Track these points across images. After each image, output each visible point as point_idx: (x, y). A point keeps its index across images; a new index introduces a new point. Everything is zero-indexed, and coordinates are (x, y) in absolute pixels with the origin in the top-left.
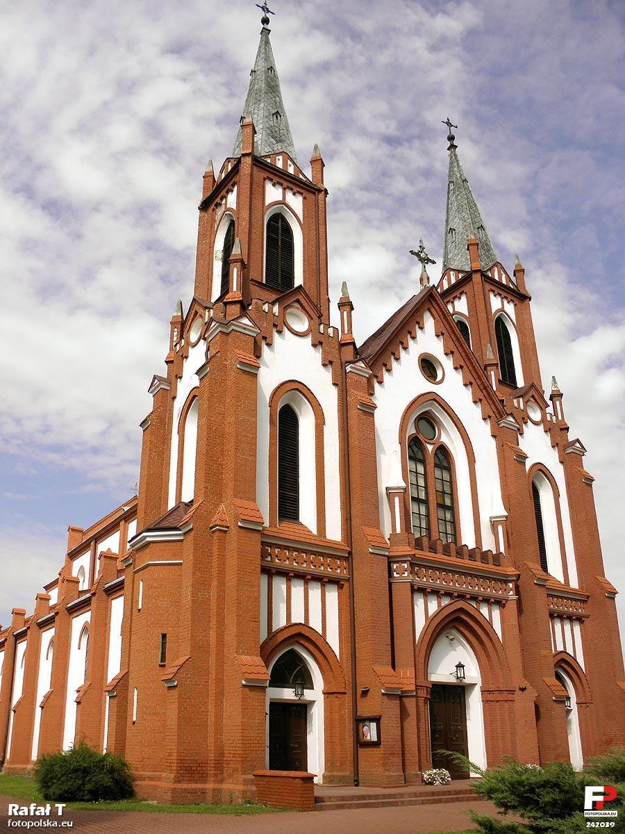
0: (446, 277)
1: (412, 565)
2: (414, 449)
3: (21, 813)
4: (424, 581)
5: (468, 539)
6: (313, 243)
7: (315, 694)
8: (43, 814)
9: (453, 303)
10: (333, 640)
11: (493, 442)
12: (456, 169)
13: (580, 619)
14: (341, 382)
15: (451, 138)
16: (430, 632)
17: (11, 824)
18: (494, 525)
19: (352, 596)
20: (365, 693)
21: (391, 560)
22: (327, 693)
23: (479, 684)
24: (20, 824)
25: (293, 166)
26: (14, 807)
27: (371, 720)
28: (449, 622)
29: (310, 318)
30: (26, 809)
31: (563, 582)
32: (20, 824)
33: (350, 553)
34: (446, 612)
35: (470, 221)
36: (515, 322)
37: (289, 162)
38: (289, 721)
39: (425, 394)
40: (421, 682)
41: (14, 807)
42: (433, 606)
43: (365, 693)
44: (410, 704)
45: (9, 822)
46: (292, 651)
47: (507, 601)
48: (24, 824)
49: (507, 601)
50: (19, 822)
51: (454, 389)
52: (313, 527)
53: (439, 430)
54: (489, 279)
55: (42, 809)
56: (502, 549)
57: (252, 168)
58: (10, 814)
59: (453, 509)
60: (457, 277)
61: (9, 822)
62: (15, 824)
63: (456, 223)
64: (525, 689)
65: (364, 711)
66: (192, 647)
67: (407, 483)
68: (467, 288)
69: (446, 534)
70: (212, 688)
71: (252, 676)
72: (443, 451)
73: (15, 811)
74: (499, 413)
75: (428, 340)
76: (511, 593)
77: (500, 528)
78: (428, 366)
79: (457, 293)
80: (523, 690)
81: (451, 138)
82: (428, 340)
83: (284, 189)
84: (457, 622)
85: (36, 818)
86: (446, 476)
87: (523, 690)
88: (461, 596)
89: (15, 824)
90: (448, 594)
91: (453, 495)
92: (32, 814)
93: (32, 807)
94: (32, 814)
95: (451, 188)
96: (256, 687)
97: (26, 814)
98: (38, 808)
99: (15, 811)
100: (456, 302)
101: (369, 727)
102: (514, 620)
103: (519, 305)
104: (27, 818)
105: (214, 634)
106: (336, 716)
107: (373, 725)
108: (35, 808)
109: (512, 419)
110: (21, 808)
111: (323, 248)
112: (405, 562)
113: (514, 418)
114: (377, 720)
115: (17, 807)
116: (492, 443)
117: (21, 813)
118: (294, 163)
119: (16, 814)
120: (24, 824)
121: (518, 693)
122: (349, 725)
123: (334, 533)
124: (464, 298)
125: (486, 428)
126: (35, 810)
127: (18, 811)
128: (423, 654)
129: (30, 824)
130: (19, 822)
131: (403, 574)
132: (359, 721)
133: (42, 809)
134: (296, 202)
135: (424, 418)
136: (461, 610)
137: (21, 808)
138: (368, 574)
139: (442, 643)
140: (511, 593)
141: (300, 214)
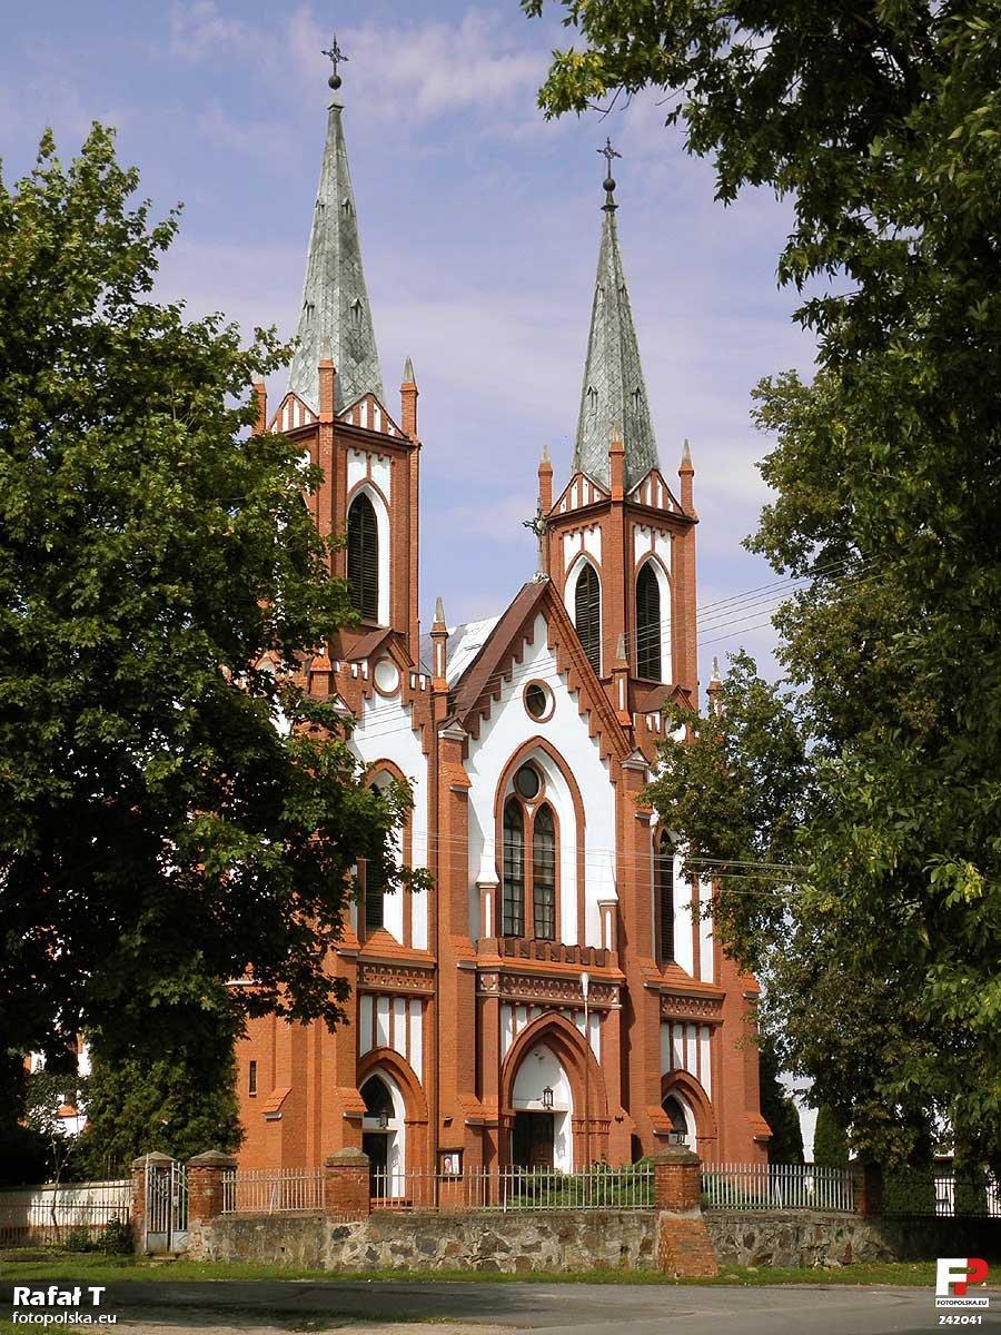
0: (576, 485)
1: (501, 975)
2: (510, 814)
3: (33, 1302)
4: (517, 993)
5: (569, 937)
6: (402, 535)
7: (398, 1124)
8: (69, 1303)
9: (582, 534)
10: (416, 1064)
11: (611, 791)
12: (610, 262)
13: (712, 1027)
14: (432, 752)
15: (610, 187)
16: (516, 1053)
17: (17, 1318)
18: (602, 906)
19: (437, 1013)
20: (448, 1123)
21: (478, 973)
22: (410, 1123)
23: (571, 1112)
24: (33, 1319)
25: (379, 411)
26: (22, 1293)
27: (453, 1152)
28: (543, 1036)
29: (401, 669)
30: (41, 1295)
31: (691, 975)
32: (33, 1319)
33: (436, 965)
34: (535, 1029)
35: (620, 383)
36: (669, 569)
37: (376, 407)
38: (377, 1147)
39: (528, 742)
40: (506, 1110)
41: (22, 1293)
42: (522, 1025)
43: (448, 1123)
44: (494, 1135)
45: (15, 1316)
46: (376, 1079)
47: (609, 1010)
48: (39, 1319)
49: (609, 1010)
50: (31, 1315)
51: (568, 727)
52: (399, 936)
53: (543, 783)
54: (639, 509)
55: (68, 1295)
56: (609, 946)
57: (334, 444)
58: (16, 1303)
59: (552, 888)
60: (591, 496)
61: (15, 1316)
62: (23, 1319)
63: (600, 381)
64: (622, 1119)
65: (445, 1143)
66: (293, 1079)
67: (500, 879)
68: (601, 520)
69: (543, 922)
70: (311, 1120)
71: (352, 1109)
72: (546, 811)
73: (24, 1297)
74: (622, 748)
75: (541, 663)
76: (615, 1000)
77: (608, 915)
78: (536, 699)
79: (589, 522)
80: (619, 1120)
81: (610, 187)
82: (541, 663)
83: (369, 458)
84: (551, 1040)
85: (57, 1309)
86: (549, 846)
87: (619, 1120)
88: (555, 1007)
89: (23, 1319)
90: (540, 1005)
91: (554, 870)
92: (51, 1303)
93: (52, 1291)
94: (51, 1303)
95: (600, 300)
96: (354, 1121)
97: (42, 1303)
98: (61, 1293)
99: (24, 1297)
100: (587, 534)
101: (450, 1159)
102: (615, 1035)
103: (678, 538)
104: (46, 1309)
105: (313, 1065)
106: (418, 1148)
107: (456, 1157)
108: (56, 1293)
109: (641, 758)
110: (35, 1294)
111: (413, 544)
112: (493, 973)
113: (642, 754)
114: (460, 1152)
115: (27, 1291)
116: (610, 792)
117: (34, 1302)
118: (381, 408)
119: (26, 1303)
120: (39, 1319)
121: (614, 1123)
122: (430, 1158)
123: (421, 941)
124: (597, 531)
125: (603, 773)
126: (56, 1297)
127: (29, 1298)
128: (508, 1077)
129: (49, 1319)
130: (31, 1315)
131: (491, 986)
132: (441, 1153)
133: (68, 1294)
134: (382, 474)
135: (526, 773)
136: (553, 1024)
137: (35, 1294)
138: (451, 990)
139: (531, 1062)
140: (615, 1000)
141: (386, 491)
